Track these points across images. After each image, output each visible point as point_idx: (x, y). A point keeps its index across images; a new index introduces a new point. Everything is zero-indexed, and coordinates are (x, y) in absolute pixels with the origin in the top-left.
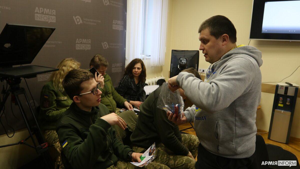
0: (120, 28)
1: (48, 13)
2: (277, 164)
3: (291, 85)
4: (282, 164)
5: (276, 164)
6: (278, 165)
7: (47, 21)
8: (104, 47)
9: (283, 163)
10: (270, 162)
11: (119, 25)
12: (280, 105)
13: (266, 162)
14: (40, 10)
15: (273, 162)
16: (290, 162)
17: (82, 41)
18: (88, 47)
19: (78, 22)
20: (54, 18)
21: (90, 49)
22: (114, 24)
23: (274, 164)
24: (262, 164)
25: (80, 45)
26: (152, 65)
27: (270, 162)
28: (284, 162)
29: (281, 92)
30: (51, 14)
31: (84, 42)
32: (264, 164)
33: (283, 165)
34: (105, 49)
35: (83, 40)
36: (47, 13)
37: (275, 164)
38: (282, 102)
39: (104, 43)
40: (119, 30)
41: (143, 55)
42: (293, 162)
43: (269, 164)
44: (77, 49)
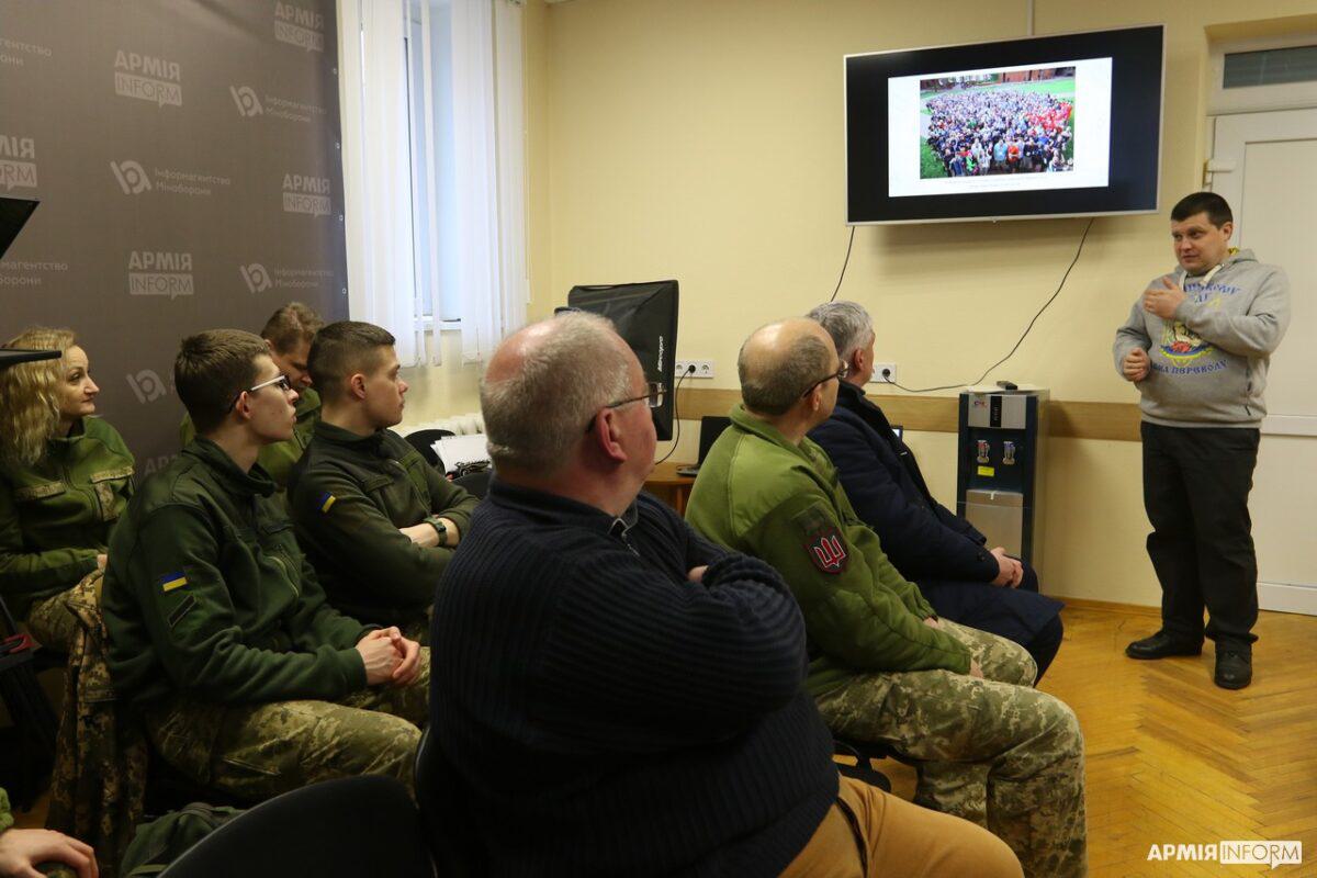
0: (319, 207)
1: (169, 266)
2: (1215, 858)
3: (1011, 388)
4: (1238, 857)
5: (1211, 857)
6: (1222, 861)
7: (167, 292)
8: (250, 285)
9: (1244, 852)
10: (1187, 846)
11: (313, 193)
12: (983, 471)
13: (1166, 847)
14: (145, 258)
15: (1201, 846)
16: (1275, 849)
17: (152, 259)
18: (184, 286)
19: (131, 186)
20: (30, 171)
21: (190, 291)
22: (288, 190)
23: (1204, 854)
24: (1151, 857)
25: (147, 275)
26: (473, 357)
27: (1187, 846)
28: (1247, 848)
29: (980, 418)
30: (16, 154)
31: (161, 263)
32: (1160, 858)
33: (1242, 861)
34: (257, 292)
35: (160, 255)
36: (165, 268)
37: (1207, 858)
38: (987, 460)
39: (251, 268)
40: (313, 215)
41: (429, 318)
42: (1285, 849)
43: (1183, 856)
44: (133, 292)
